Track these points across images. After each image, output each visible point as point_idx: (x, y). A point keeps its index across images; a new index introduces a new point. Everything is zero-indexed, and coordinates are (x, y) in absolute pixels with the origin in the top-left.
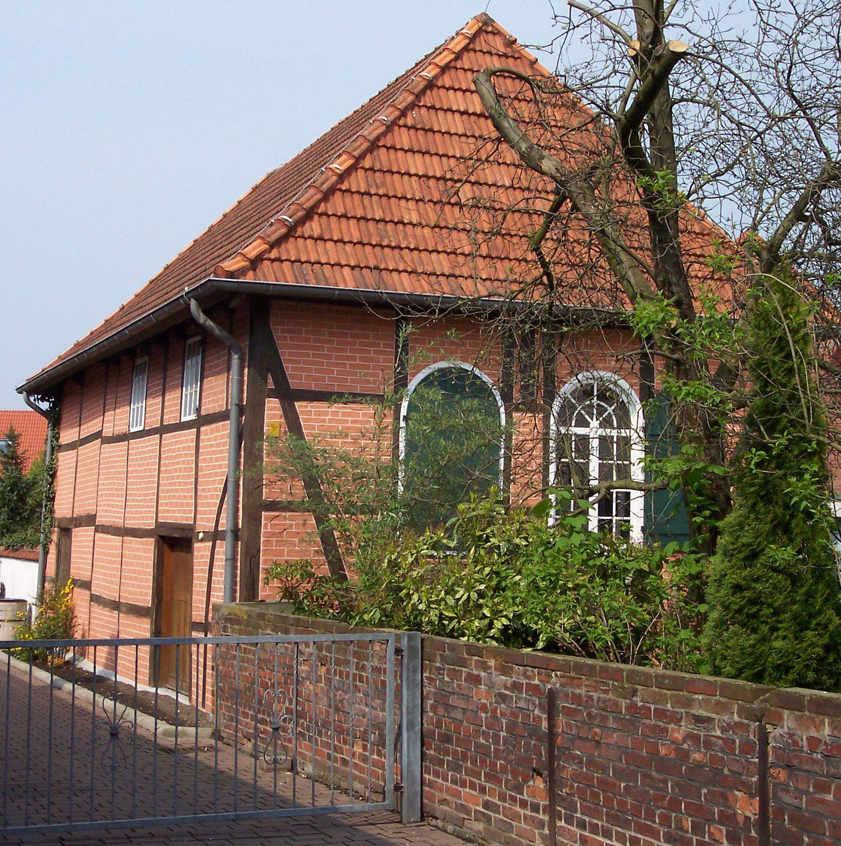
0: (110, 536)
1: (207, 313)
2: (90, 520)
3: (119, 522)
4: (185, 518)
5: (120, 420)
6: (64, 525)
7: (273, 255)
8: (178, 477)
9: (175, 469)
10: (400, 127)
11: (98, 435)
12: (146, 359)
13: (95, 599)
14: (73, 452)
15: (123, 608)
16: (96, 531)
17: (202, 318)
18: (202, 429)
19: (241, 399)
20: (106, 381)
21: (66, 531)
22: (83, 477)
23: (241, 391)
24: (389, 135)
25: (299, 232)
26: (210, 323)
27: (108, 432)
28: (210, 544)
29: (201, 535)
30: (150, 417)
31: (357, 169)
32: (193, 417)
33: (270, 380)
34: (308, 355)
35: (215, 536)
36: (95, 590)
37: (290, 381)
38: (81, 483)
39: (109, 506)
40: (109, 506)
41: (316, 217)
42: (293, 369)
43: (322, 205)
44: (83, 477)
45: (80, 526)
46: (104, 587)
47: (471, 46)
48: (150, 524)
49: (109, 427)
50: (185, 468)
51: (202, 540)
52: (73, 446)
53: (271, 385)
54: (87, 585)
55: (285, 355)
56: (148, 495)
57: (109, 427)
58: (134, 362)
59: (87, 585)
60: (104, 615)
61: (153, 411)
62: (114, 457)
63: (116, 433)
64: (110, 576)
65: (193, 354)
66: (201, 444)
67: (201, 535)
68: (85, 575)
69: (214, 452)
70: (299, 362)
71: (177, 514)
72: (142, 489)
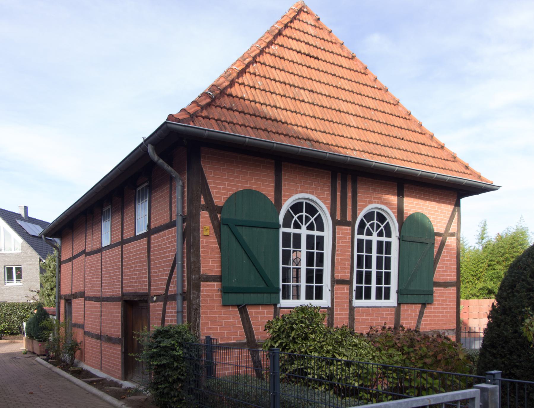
0: (93, 302)
1: (160, 156)
2: (81, 295)
3: (99, 295)
4: (141, 288)
5: (95, 242)
6: (67, 298)
7: (205, 113)
8: (136, 267)
9: (133, 263)
10: (266, 53)
11: (84, 252)
12: (110, 207)
13: (85, 333)
14: (70, 263)
15: (103, 339)
16: (85, 300)
17: (155, 158)
18: (152, 237)
19: (183, 212)
20: (86, 224)
21: (68, 302)
22: (76, 274)
23: (183, 207)
24: (261, 56)
25: (218, 102)
26: (161, 161)
27: (89, 249)
28: (162, 303)
29: (155, 298)
30: (114, 237)
31: (245, 73)
32: (145, 231)
33: (202, 199)
34: (225, 184)
35: (166, 298)
36: (86, 329)
37: (214, 200)
38: (75, 277)
39: (92, 287)
40: (92, 287)
41: (237, 85)
42: (216, 193)
43: (229, 89)
44: (76, 274)
45: (76, 298)
46: (92, 326)
47: (297, 17)
48: (118, 293)
49: (90, 247)
50: (140, 261)
51: (155, 301)
52: (70, 260)
53: (203, 202)
54: (82, 326)
55: (211, 184)
56: (116, 279)
57: (90, 247)
58: (102, 210)
59: (82, 326)
60: (92, 342)
61: (116, 234)
62: (93, 261)
63: (94, 249)
64: (95, 322)
65: (141, 198)
66: (152, 246)
67: (155, 298)
68: (81, 321)
69: (162, 249)
70: (219, 189)
71: (136, 286)
72: (112, 276)
